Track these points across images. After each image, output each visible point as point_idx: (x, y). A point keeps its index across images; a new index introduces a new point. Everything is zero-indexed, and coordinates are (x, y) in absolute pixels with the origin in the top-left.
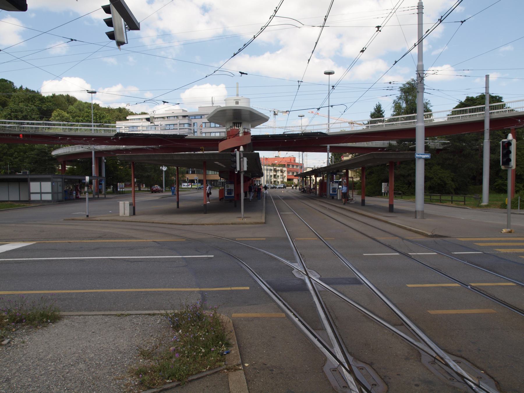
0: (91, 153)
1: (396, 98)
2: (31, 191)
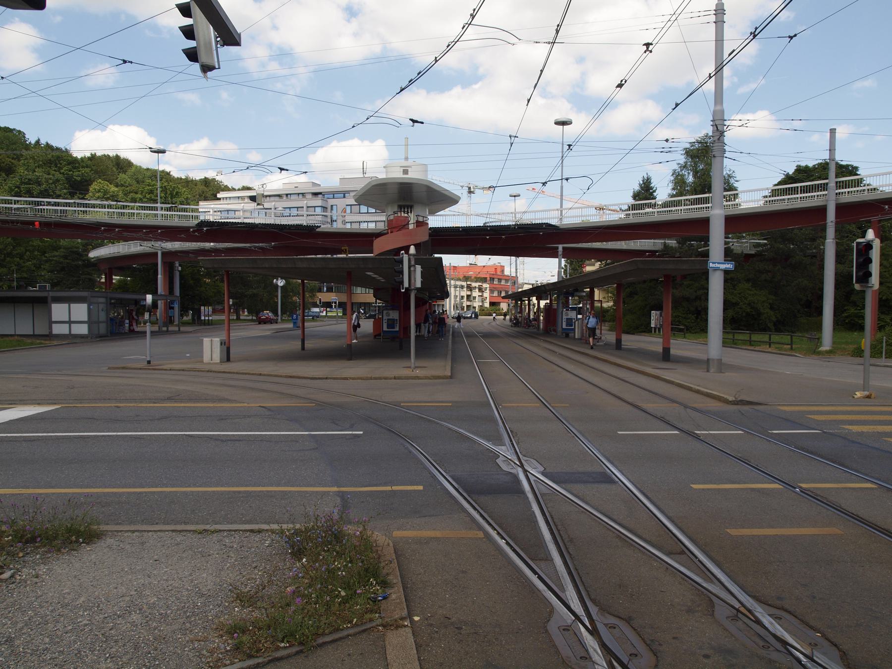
0: (157, 254)
1: (676, 167)
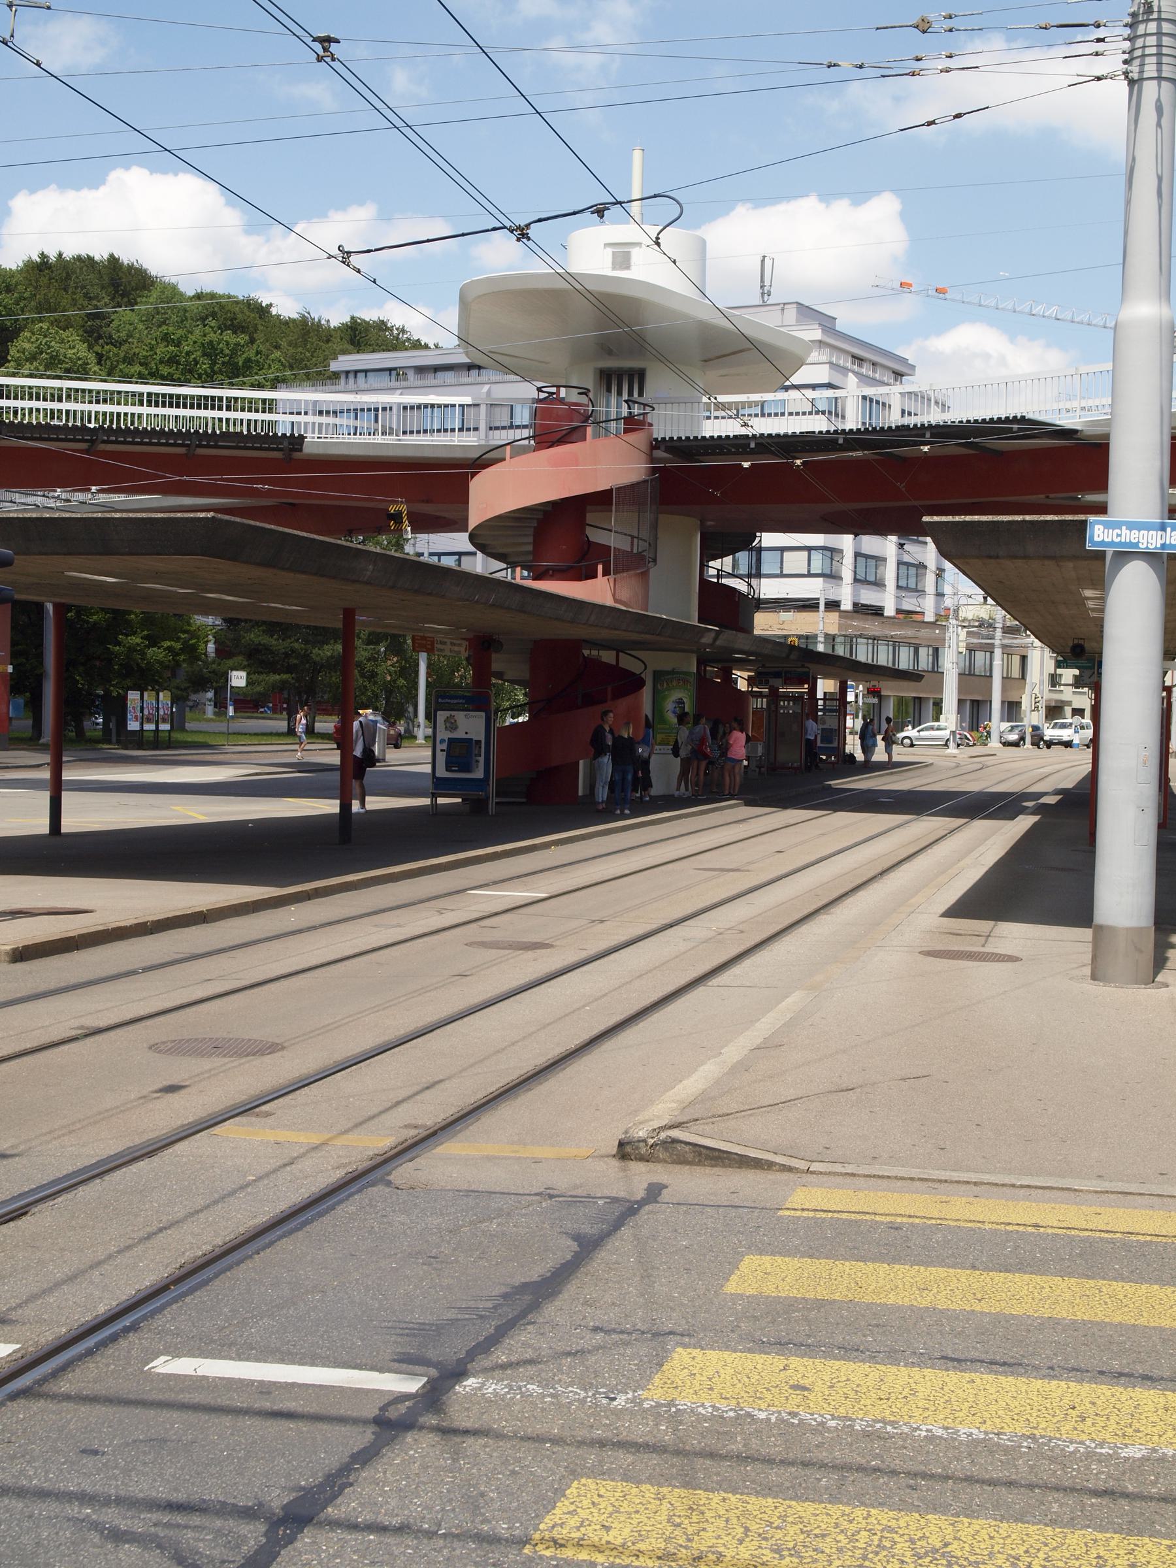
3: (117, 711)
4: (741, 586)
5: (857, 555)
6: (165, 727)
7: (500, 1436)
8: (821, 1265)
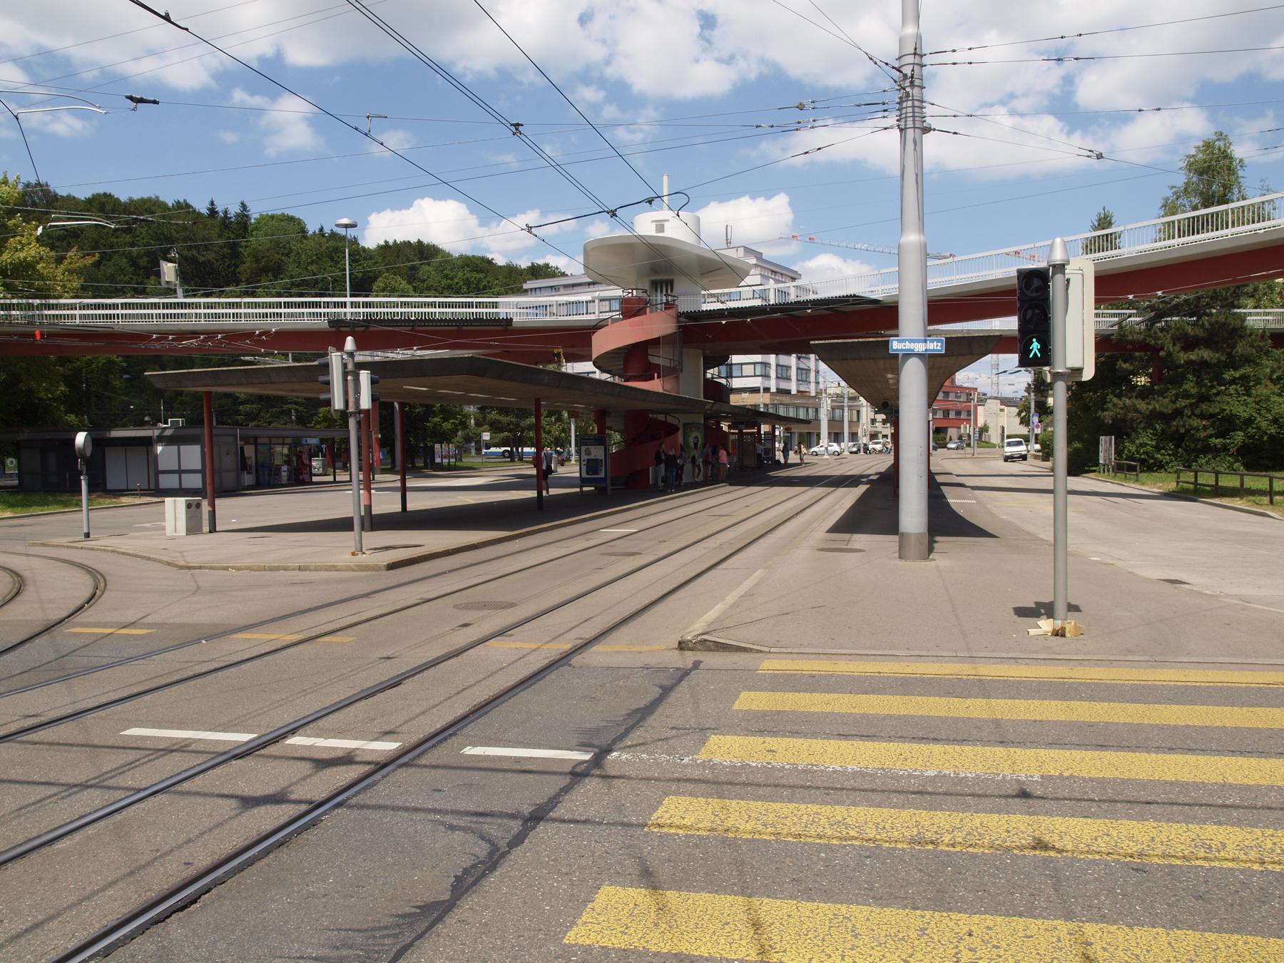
1: (1169, 193)
2: (160, 468)
3: (431, 452)
4: (723, 381)
5: (777, 365)
6: (453, 460)
7: (629, 778)
8: (779, 695)
